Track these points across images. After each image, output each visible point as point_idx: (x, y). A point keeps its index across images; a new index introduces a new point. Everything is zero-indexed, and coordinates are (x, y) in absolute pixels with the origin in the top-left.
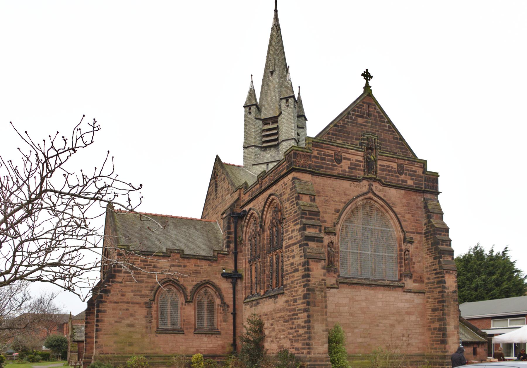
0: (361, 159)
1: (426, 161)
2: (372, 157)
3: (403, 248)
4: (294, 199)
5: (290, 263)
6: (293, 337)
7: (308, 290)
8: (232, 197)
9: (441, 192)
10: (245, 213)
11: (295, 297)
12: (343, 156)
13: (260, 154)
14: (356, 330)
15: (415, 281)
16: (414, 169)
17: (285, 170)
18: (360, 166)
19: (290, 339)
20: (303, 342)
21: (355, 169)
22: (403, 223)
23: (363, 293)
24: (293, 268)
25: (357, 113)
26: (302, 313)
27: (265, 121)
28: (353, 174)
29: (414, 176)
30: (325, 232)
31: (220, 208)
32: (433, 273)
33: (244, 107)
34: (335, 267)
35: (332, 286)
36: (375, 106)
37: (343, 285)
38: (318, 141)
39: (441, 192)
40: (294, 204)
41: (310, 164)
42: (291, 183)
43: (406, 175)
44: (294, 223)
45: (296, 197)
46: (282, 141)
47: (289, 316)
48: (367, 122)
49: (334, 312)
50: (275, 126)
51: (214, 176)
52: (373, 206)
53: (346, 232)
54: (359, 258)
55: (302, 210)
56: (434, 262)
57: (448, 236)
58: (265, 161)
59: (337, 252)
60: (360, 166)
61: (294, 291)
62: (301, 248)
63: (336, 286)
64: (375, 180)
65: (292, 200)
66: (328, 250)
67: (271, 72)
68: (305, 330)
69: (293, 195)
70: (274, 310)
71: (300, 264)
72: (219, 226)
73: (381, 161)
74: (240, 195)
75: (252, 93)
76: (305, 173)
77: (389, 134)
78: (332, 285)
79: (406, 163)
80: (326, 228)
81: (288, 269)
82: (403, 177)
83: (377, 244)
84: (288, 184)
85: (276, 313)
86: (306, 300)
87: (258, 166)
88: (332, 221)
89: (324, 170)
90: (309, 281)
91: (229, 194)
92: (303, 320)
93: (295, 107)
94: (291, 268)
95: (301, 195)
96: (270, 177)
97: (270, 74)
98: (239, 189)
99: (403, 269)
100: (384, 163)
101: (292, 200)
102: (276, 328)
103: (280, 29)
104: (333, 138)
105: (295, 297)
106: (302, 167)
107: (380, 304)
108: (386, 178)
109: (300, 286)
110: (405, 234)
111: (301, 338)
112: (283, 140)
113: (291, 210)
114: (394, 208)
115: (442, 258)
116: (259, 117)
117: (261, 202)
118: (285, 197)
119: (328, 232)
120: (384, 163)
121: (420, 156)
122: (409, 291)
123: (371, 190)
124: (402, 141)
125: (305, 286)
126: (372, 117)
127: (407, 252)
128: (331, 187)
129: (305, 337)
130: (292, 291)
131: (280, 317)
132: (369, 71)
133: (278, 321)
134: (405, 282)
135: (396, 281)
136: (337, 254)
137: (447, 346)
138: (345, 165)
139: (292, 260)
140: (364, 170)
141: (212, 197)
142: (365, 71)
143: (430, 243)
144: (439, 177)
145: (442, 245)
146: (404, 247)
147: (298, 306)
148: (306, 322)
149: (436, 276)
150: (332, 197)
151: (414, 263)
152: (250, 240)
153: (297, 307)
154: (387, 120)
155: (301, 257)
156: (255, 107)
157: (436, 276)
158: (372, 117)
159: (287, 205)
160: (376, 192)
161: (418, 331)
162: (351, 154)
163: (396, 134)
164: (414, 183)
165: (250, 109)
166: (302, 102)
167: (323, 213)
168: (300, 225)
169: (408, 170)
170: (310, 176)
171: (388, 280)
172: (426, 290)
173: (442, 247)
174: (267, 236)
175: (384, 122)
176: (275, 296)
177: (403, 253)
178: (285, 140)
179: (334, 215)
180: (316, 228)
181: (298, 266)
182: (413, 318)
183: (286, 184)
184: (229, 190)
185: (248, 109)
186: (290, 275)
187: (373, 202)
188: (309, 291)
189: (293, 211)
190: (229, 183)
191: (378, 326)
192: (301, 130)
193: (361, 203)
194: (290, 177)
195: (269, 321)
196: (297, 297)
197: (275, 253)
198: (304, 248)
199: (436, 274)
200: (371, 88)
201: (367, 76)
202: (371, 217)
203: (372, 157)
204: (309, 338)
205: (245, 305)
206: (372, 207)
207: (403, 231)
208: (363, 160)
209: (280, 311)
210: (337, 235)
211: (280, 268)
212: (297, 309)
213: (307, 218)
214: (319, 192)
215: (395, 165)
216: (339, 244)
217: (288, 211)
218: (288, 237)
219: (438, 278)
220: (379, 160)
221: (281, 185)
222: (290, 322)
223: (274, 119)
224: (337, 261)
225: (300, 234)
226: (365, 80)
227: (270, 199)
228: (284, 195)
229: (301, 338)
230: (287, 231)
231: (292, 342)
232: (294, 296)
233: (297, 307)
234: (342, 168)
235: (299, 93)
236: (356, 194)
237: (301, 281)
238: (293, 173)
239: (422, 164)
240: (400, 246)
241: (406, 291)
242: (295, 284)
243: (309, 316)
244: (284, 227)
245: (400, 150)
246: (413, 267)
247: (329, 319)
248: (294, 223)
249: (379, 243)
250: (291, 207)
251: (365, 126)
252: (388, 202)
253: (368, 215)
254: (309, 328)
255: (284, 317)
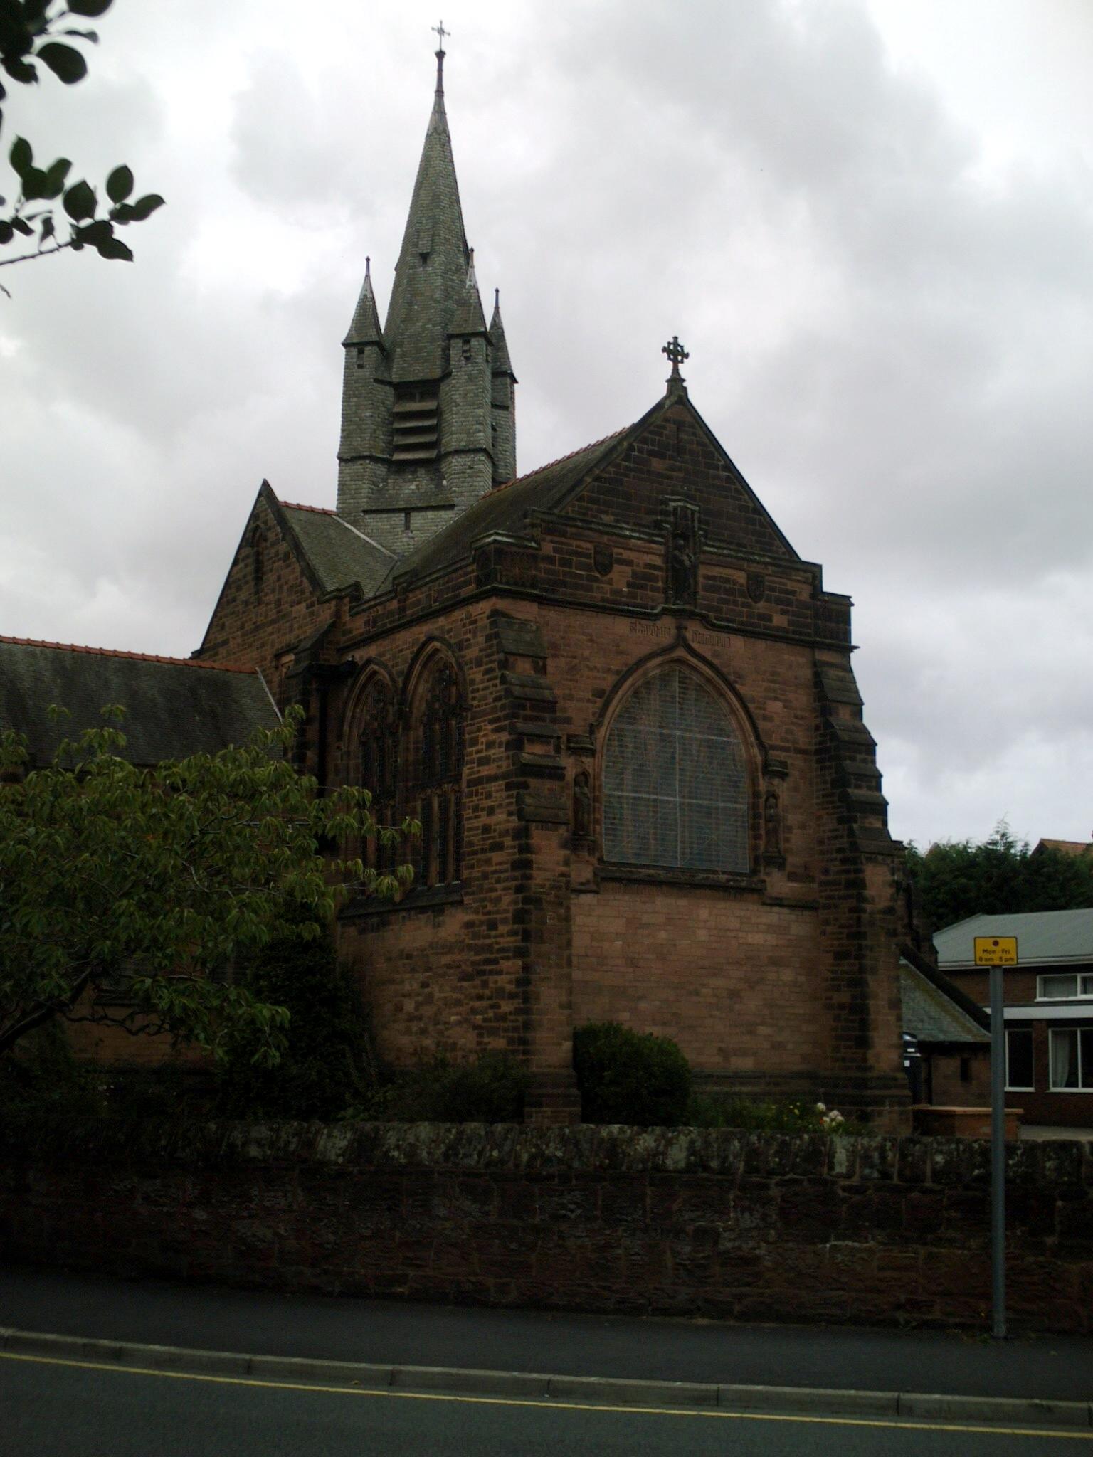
0: (658, 561)
1: (819, 567)
2: (685, 558)
3: (761, 788)
4: (495, 665)
5: (480, 824)
6: (485, 1020)
7: (526, 901)
8: (312, 614)
9: (856, 647)
10: (353, 669)
11: (492, 916)
12: (614, 556)
13: (385, 480)
14: (643, 1005)
15: (792, 877)
16: (790, 585)
17: (473, 586)
18: (655, 579)
19: (476, 1027)
20: (511, 1034)
21: (643, 587)
22: (761, 725)
23: (661, 906)
24: (489, 838)
25: (650, 447)
26: (508, 958)
27: (404, 390)
28: (639, 601)
29: (789, 603)
30: (569, 748)
31: (272, 634)
32: (836, 859)
33: (345, 345)
34: (592, 838)
35: (583, 887)
36: (693, 427)
37: (611, 885)
38: (555, 519)
39: (856, 647)
40: (495, 678)
41: (535, 576)
42: (487, 622)
43: (768, 600)
44: (494, 726)
45: (499, 661)
46: (450, 453)
47: (473, 963)
48: (672, 468)
49: (587, 956)
50: (430, 405)
51: (254, 536)
52: (688, 681)
53: (621, 746)
54: (651, 814)
55: (517, 698)
56: (837, 830)
57: (874, 762)
58: (402, 504)
59: (596, 799)
60: (655, 579)
61: (491, 900)
62: (510, 793)
63: (594, 887)
64: (691, 615)
65: (490, 666)
66: (575, 794)
67: (421, 254)
68: (517, 1003)
69: (492, 654)
70: (431, 945)
71: (507, 831)
72: (265, 685)
73: (708, 567)
74: (338, 614)
75: (367, 306)
76: (524, 599)
77: (726, 497)
78: (582, 884)
79: (770, 572)
80: (570, 738)
81: (476, 840)
82: (761, 606)
83: (697, 777)
84: (479, 624)
85: (437, 954)
86: (521, 926)
87: (379, 516)
88: (585, 720)
89: (569, 591)
90: (530, 878)
91: (304, 605)
92: (513, 977)
93: (487, 361)
94: (484, 839)
95: (511, 659)
96: (430, 590)
97: (417, 261)
98: (338, 596)
99: (762, 843)
100: (716, 571)
101: (490, 666)
102: (437, 995)
103: (449, 141)
104: (592, 510)
105: (492, 916)
106: (516, 584)
107: (702, 935)
108: (719, 610)
109: (505, 889)
110: (766, 754)
111: (505, 1025)
112: (451, 449)
113: (487, 692)
114: (738, 686)
115: (856, 822)
116: (386, 377)
117: (401, 651)
118: (473, 653)
119: (579, 748)
120: (716, 571)
121: (805, 555)
122: (778, 902)
123: (681, 641)
124: (760, 514)
125: (519, 889)
126: (687, 457)
127: (772, 801)
128: (584, 634)
129: (517, 1021)
130: (484, 900)
131: (449, 966)
132: (680, 342)
133: (443, 976)
134: (767, 879)
135: (745, 875)
136: (597, 805)
137: (870, 1053)
138: (619, 578)
139: (485, 819)
140: (665, 590)
141: (243, 596)
142: (672, 341)
143: (828, 778)
144: (852, 608)
145: (858, 787)
146: (763, 785)
147: (498, 940)
148: (519, 983)
149: (844, 867)
150: (587, 659)
151: (789, 829)
152: (364, 744)
153: (498, 943)
154: (723, 463)
155: (510, 814)
156: (375, 349)
157: (844, 867)
158: (687, 457)
159: (477, 675)
160: (695, 646)
161: (801, 1011)
162: (635, 551)
163: (746, 496)
164: (790, 622)
165: (361, 352)
166: (503, 332)
167: (564, 698)
168: (510, 734)
169: (773, 589)
170: (535, 607)
171: (724, 873)
172: (822, 901)
173: (857, 791)
174: (416, 742)
175: (717, 468)
176: (438, 909)
177: (762, 801)
178: (457, 452)
179: (590, 705)
180: (548, 743)
181: (501, 835)
182: (788, 975)
183: (475, 622)
184: (303, 592)
185: (354, 351)
186: (479, 856)
187: (687, 671)
188: (528, 903)
189: (491, 693)
190: (302, 573)
191: (698, 994)
192: (502, 413)
193: (657, 671)
194: (484, 607)
195: (417, 975)
196: (498, 916)
197: (439, 792)
198: (518, 794)
199: (844, 861)
200: (685, 384)
201: (675, 352)
202: (681, 709)
203: (685, 558)
204: (527, 1026)
205: (343, 926)
206: (684, 683)
207: (761, 745)
208: (663, 565)
209: (449, 948)
210: (598, 755)
211: (451, 832)
212: (496, 947)
213: (526, 718)
214: (554, 646)
215: (741, 577)
216: (603, 778)
217: (478, 690)
218: (475, 756)
219: (848, 872)
220: (703, 563)
221: (462, 620)
222: (477, 982)
223: (429, 388)
224: (597, 822)
225: (508, 758)
226: (671, 363)
227: (429, 649)
228: (468, 647)
229: (505, 1025)
230: (474, 742)
231: (480, 1035)
232: (489, 913)
233: (498, 943)
234: (611, 584)
235: (497, 308)
236: (645, 650)
237: (506, 875)
238: (494, 600)
239: (810, 575)
240: (754, 783)
241: (768, 901)
242: (493, 881)
243: (526, 968)
244: (468, 729)
245: (754, 538)
246: (787, 840)
247: (577, 975)
248: (494, 726)
249: (702, 775)
250: (486, 684)
251: (670, 478)
252: (725, 670)
253: (674, 702)
254: (526, 1000)
255: (459, 967)
